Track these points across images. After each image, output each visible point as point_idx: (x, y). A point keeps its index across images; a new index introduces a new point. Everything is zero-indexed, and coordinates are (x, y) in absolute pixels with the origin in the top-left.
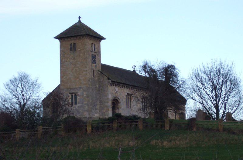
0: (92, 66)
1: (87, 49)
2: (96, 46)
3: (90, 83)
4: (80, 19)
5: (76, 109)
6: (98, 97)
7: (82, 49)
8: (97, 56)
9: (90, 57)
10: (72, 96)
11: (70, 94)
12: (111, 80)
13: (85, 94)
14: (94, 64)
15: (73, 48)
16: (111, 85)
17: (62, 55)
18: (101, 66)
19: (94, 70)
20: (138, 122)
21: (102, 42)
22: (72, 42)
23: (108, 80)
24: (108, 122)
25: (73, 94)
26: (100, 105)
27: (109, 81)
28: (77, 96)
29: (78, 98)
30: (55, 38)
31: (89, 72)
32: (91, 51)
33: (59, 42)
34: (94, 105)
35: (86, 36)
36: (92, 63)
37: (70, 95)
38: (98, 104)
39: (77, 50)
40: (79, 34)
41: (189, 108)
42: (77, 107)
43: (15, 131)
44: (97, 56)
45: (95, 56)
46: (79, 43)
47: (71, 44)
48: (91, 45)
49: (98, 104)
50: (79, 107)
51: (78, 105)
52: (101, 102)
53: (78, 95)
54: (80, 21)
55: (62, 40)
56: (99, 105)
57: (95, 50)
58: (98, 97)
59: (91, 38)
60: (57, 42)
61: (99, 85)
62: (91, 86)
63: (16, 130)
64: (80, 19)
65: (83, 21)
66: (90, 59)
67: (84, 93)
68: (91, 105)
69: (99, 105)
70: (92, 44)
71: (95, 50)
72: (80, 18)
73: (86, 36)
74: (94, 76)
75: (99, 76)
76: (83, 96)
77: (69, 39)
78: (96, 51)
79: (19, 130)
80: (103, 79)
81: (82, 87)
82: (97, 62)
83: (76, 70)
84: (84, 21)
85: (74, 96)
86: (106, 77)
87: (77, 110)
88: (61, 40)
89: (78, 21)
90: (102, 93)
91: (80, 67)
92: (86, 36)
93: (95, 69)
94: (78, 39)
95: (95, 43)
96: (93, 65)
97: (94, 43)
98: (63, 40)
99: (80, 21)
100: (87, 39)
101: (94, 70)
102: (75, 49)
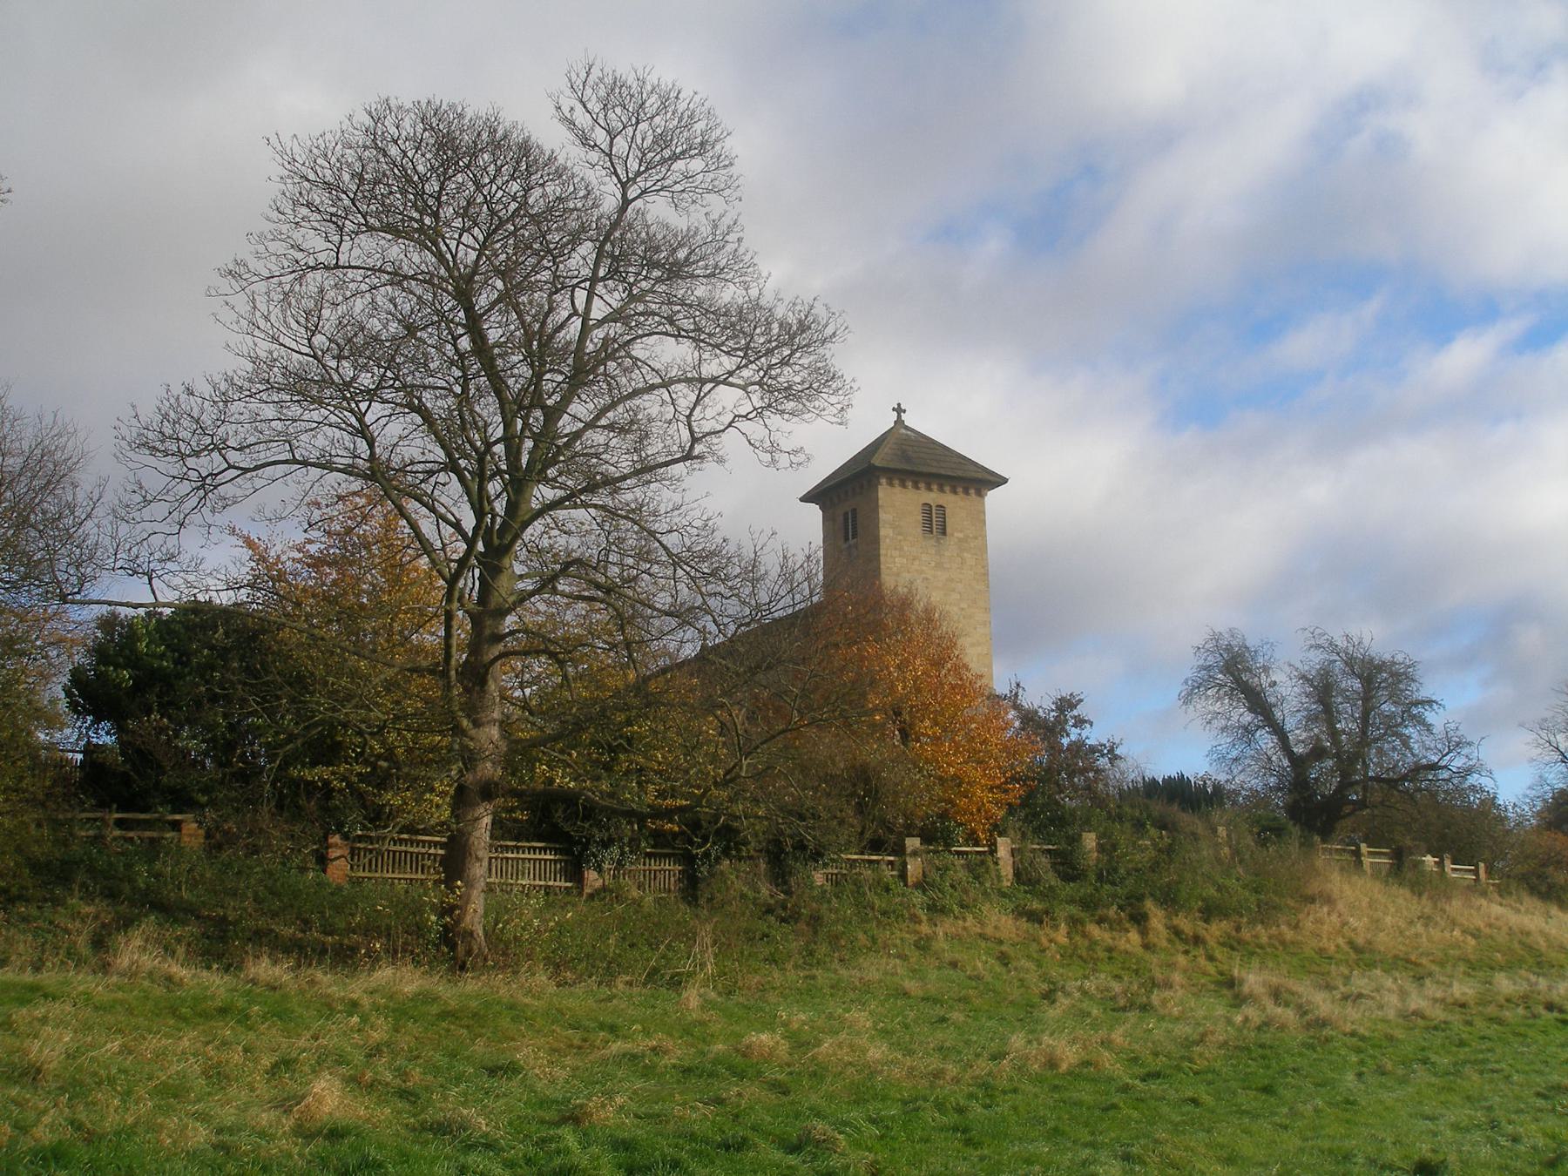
4: (899, 416)
21: (993, 497)
22: (933, 497)
54: (899, 422)
64: (899, 416)
65: (908, 419)
84: (927, 422)
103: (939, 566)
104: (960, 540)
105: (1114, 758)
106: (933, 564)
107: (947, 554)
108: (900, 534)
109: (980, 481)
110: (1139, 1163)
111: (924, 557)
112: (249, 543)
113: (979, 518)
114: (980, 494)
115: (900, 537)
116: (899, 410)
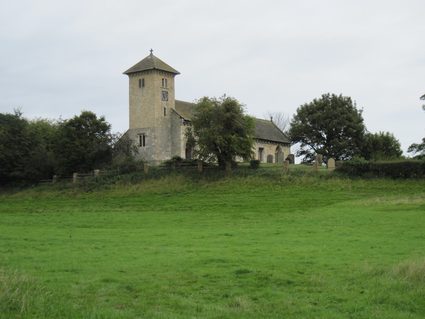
0: (162, 104)
1: (156, 85)
2: (169, 82)
3: (159, 122)
4: (151, 52)
5: (144, 151)
6: (170, 138)
7: (150, 85)
8: (170, 92)
9: (160, 94)
10: (141, 137)
11: (138, 134)
12: (184, 119)
13: (153, 135)
14: (166, 102)
15: (142, 84)
16: (185, 125)
17: (131, 92)
18: (174, 103)
19: (165, 108)
20: (197, 165)
21: (176, 77)
22: (141, 77)
23: (180, 119)
24: (165, 165)
25: (141, 135)
26: (173, 147)
27: (181, 120)
28: (145, 137)
29: (146, 139)
30: (124, 73)
31: (159, 110)
32: (162, 87)
33: (129, 78)
34: (165, 147)
35: (154, 70)
36: (163, 100)
37: (139, 136)
38: (170, 145)
39: (146, 86)
40: (148, 68)
41: (3, 122)
42: (145, 149)
43: (73, 175)
44: (170, 92)
45: (167, 92)
46: (147, 78)
47: (140, 80)
48: (162, 81)
49: (170, 145)
50: (147, 149)
51: (146, 147)
52: (173, 144)
53: (146, 136)
54: (151, 54)
55: (146, 73)
56: (171, 146)
57: (166, 86)
58: (170, 138)
59: (161, 73)
60: (127, 77)
61: (172, 124)
62: (160, 126)
63: (74, 174)
64: (151, 52)
65: (155, 54)
66: (159, 96)
67: (152, 133)
68: (160, 147)
69: (171, 146)
70: (163, 79)
71: (166, 86)
72: (151, 51)
73: (154, 71)
74: (165, 115)
75: (171, 115)
76: (151, 137)
77: (138, 74)
78: (168, 87)
79: (76, 174)
80: (176, 118)
81: (150, 127)
82: (169, 99)
83: (144, 108)
84: (159, 55)
85: (143, 137)
86: (178, 115)
87: (145, 153)
88: (130, 75)
89: (149, 55)
90: (174, 134)
91: (148, 105)
92: (154, 71)
93: (166, 107)
94: (138, 76)
95: (167, 78)
96: (163, 102)
97: (166, 78)
98: (132, 75)
99: (151, 54)
100: (156, 73)
101: (165, 108)
102: (143, 86)
103: (143, 96)
104: (148, 87)
105: (230, 98)
106: (141, 96)
107: (144, 92)
108: (134, 89)
109: (173, 73)
110: (172, 149)
111: (139, 94)
112: (49, 271)
113: (173, 81)
114: (174, 77)
115: (134, 90)
116: (151, 51)
